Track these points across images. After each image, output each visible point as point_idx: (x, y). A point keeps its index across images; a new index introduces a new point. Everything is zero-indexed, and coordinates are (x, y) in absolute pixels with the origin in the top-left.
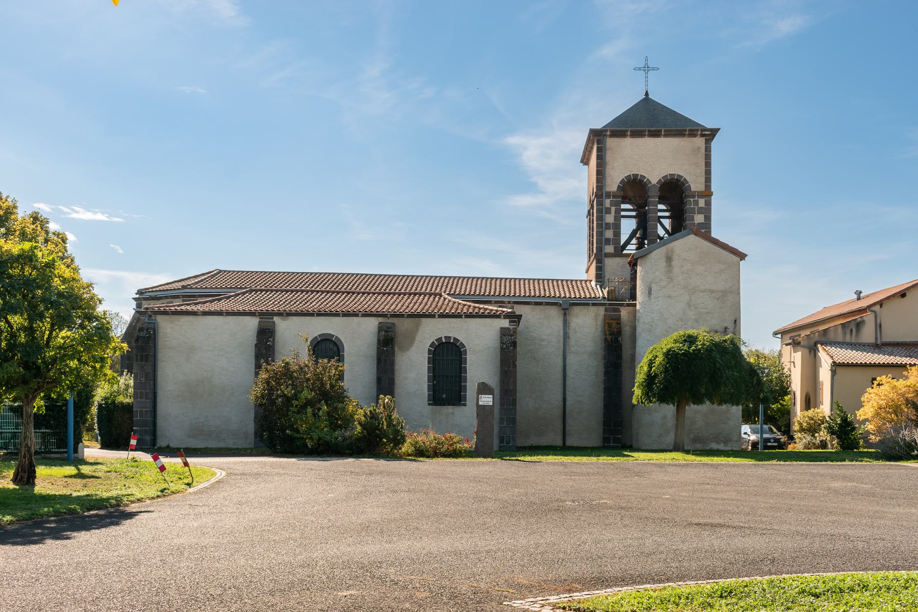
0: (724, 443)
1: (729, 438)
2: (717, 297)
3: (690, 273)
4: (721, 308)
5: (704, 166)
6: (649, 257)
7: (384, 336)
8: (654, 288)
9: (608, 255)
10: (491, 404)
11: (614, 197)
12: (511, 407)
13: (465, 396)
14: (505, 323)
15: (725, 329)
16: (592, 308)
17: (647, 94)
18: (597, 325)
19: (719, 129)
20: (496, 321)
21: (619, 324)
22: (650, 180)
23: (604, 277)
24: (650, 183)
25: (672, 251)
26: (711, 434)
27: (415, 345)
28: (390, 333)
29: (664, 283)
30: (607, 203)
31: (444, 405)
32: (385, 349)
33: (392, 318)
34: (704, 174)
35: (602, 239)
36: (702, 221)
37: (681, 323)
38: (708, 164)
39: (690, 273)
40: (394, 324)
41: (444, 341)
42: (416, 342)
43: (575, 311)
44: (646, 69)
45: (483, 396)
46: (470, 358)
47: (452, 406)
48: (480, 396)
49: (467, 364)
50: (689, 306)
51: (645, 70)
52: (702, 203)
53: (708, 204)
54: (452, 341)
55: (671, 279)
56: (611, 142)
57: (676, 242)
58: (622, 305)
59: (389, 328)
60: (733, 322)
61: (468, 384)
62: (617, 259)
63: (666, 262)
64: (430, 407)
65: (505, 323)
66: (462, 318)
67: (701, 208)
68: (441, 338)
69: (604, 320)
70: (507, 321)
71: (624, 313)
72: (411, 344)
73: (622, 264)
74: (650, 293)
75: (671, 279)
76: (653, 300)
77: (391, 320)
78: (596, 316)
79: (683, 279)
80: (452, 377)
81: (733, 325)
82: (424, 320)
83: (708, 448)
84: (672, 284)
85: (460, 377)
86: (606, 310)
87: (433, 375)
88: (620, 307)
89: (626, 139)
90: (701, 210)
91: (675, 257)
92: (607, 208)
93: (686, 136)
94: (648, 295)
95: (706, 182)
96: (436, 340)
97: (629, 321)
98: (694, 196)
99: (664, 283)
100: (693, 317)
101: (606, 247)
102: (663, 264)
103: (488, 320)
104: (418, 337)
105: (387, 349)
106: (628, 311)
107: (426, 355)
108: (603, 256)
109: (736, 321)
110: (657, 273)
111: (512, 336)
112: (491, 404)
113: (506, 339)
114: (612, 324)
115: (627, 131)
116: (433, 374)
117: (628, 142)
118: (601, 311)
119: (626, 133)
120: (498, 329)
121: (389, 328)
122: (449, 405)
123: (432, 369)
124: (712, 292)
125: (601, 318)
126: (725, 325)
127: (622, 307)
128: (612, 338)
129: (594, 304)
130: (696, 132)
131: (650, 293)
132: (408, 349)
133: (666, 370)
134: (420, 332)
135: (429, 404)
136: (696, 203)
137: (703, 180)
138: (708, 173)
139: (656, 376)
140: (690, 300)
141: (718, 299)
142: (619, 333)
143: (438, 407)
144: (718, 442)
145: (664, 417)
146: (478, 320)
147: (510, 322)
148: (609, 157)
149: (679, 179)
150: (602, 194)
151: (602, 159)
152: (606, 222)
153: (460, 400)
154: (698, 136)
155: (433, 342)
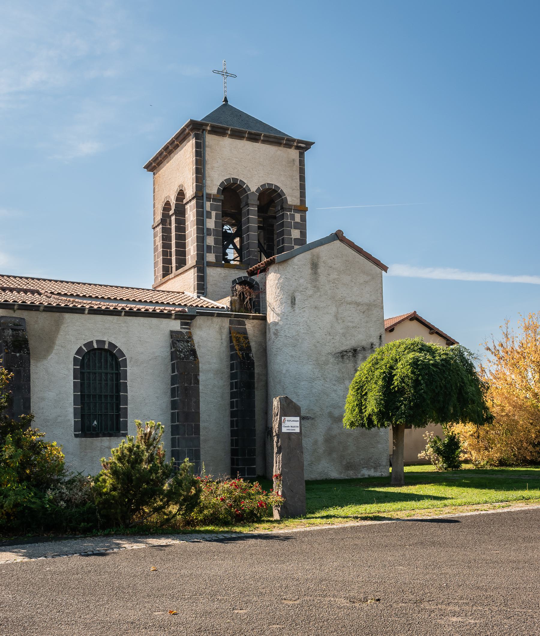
0: (375, 468)
1: (379, 463)
2: (362, 311)
3: (337, 282)
4: (367, 322)
5: (299, 180)
6: (290, 262)
7: (13, 336)
8: (299, 297)
9: (210, 264)
10: (298, 430)
11: (215, 200)
12: (194, 436)
13: (126, 422)
14: (176, 325)
15: (372, 345)
16: (216, 320)
17: (226, 100)
18: (221, 339)
19: (314, 143)
20: (165, 321)
21: (246, 338)
22: (250, 187)
23: (207, 288)
24: (249, 190)
25: (318, 257)
26: (362, 459)
27: (54, 351)
28: (20, 333)
29: (310, 292)
30: (208, 205)
31: (97, 436)
32: (18, 355)
33: (20, 311)
34: (299, 188)
35: (204, 245)
36: (298, 236)
37: (329, 337)
38: (302, 179)
39: (337, 282)
40: (24, 319)
41: (96, 346)
42: (56, 347)
43: (198, 322)
44: (225, 74)
45: (287, 418)
46: (131, 370)
47: (108, 438)
48: (283, 418)
49: (128, 379)
50: (337, 319)
51: (226, 73)
52: (298, 217)
53: (303, 219)
54: (106, 347)
55: (317, 288)
56: (210, 139)
57: (322, 247)
58: (247, 317)
59: (17, 325)
60: (379, 337)
61: (129, 407)
62: (219, 270)
63: (312, 269)
64: (78, 439)
65: (176, 325)
66: (120, 315)
67: (297, 223)
68: (92, 342)
69: (230, 333)
70: (178, 322)
71: (250, 326)
72: (49, 350)
73: (223, 275)
74: (293, 302)
75: (317, 288)
76: (297, 311)
77: (19, 314)
78: (221, 329)
79: (330, 289)
80: (106, 396)
81: (378, 341)
82: (67, 316)
83: (359, 476)
84: (319, 293)
85: (118, 397)
86: (231, 322)
87: (81, 394)
88: (244, 320)
89: (225, 138)
90: (297, 226)
91: (321, 265)
92: (207, 212)
93: (282, 146)
94: (290, 304)
95: (301, 197)
96: (85, 345)
97: (254, 336)
98: (290, 210)
99: (310, 292)
100: (341, 331)
101: (208, 254)
102: (307, 271)
103: (154, 321)
104: (59, 341)
105: (20, 355)
106: (253, 325)
107: (71, 367)
108: (205, 265)
109: (381, 337)
110: (302, 281)
111: (188, 342)
112: (298, 430)
113: (182, 346)
114: (240, 338)
115: (228, 129)
116: (81, 393)
117: (227, 142)
118: (226, 323)
119: (227, 132)
120: (167, 333)
121: (17, 325)
122: (104, 435)
123: (79, 386)
124: (358, 304)
125: (226, 331)
126: (371, 340)
127: (248, 320)
128: (242, 354)
129: (219, 315)
130: (292, 143)
131: (293, 302)
132: (45, 357)
133: (416, 383)
134: (61, 333)
135: (76, 436)
136: (293, 217)
137: (298, 194)
138: (302, 187)
139: (401, 391)
140: (338, 312)
141: (364, 312)
142: (249, 348)
143: (89, 439)
144: (369, 468)
145: (316, 442)
146: (142, 320)
147: (182, 324)
148: (209, 155)
149: (277, 190)
150: (203, 196)
151: (201, 156)
152: (207, 227)
153: (118, 429)
154: (293, 148)
155: (81, 347)
